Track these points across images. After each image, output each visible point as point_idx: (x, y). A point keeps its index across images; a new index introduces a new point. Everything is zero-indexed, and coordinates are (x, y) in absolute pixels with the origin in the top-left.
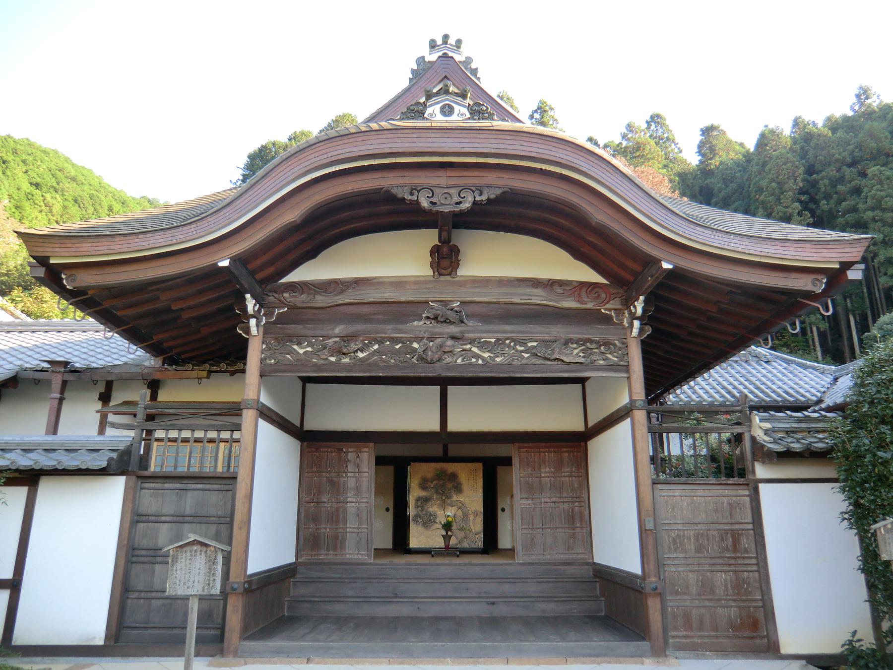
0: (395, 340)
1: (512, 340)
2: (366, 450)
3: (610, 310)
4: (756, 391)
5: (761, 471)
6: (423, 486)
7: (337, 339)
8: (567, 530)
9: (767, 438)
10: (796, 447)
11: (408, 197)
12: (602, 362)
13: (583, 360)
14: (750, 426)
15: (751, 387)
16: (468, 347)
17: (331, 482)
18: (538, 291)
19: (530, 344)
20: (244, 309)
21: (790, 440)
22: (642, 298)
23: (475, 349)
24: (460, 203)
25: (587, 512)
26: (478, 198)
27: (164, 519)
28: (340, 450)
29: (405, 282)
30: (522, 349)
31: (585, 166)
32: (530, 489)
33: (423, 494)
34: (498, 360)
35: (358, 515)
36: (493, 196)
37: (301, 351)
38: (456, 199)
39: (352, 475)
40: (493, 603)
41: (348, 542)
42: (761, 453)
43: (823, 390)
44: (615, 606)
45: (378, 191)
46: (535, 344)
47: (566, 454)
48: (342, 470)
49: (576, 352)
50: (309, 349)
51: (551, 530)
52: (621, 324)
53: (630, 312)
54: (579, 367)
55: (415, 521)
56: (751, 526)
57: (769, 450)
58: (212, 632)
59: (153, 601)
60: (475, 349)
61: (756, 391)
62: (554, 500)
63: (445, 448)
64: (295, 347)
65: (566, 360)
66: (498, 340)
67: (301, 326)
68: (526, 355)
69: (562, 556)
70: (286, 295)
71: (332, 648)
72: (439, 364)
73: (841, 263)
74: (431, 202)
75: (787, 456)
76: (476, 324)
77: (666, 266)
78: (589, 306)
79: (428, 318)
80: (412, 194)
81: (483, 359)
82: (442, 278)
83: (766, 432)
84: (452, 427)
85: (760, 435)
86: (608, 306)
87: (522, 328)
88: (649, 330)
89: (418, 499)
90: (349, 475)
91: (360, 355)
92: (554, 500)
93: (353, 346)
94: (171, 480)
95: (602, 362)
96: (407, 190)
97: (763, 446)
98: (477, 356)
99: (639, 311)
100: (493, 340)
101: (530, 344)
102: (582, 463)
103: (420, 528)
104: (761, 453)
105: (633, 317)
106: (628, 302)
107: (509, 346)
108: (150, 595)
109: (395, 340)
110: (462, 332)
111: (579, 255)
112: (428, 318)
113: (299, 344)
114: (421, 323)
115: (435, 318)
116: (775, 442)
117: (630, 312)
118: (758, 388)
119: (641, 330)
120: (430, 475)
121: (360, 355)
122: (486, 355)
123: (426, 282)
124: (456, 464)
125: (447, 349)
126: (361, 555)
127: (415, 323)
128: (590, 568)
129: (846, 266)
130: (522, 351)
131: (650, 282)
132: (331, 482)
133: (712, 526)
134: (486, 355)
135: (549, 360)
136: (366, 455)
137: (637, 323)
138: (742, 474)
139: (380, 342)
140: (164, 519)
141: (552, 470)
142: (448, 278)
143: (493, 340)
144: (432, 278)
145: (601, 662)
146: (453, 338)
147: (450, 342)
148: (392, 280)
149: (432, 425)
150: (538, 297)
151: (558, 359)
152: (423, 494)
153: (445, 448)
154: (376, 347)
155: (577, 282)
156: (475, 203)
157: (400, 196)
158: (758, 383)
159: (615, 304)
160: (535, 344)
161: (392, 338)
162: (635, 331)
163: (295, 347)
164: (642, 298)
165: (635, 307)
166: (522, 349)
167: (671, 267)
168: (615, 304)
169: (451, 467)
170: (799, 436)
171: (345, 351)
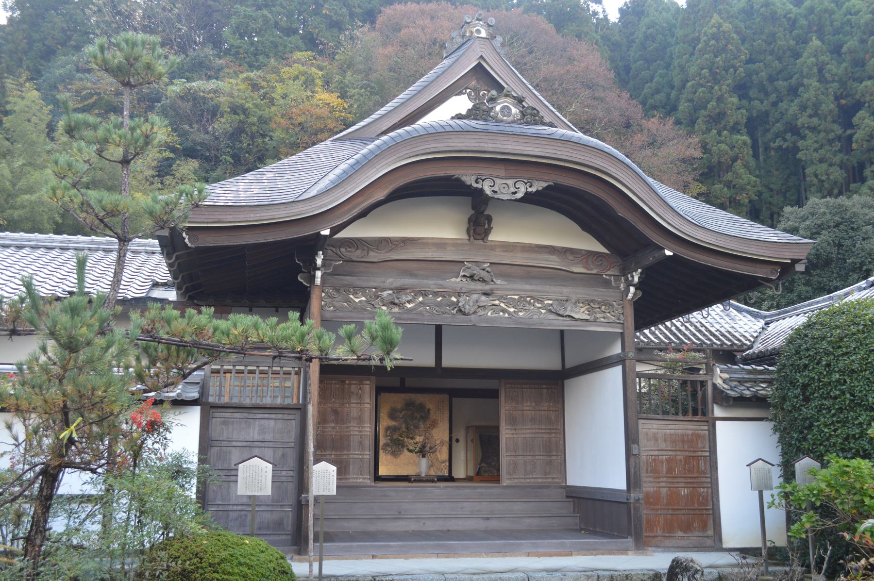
0: (436, 294)
1: (532, 297)
2: (368, 382)
3: (610, 275)
4: (698, 334)
5: (718, 412)
6: (392, 416)
7: (391, 292)
8: (545, 458)
9: (726, 386)
10: (747, 393)
11: (475, 185)
12: (602, 320)
13: (588, 317)
14: (712, 376)
15: (692, 329)
16: (497, 302)
17: (335, 412)
18: (554, 258)
19: (546, 302)
20: (314, 261)
21: (743, 388)
22: (640, 270)
23: (502, 305)
24: (515, 193)
25: (561, 442)
26: (530, 190)
27: (234, 444)
28: (343, 382)
29: (445, 244)
30: (539, 305)
31: (612, 170)
32: (513, 421)
33: (392, 423)
34: (521, 314)
35: (360, 443)
36: (540, 188)
37: (357, 300)
38: (513, 190)
39: (354, 405)
40: (488, 519)
41: (351, 467)
42: (722, 398)
43: (755, 335)
44: (597, 517)
45: (448, 178)
46: (550, 302)
47: (545, 391)
48: (345, 401)
49: (583, 309)
50: (363, 299)
51: (531, 458)
52: (618, 287)
53: (627, 279)
54: (584, 323)
55: (384, 449)
56: (708, 454)
57: (727, 395)
58: (284, 537)
59: (231, 513)
60: (502, 305)
61: (698, 334)
62: (534, 431)
63: (403, 381)
64: (351, 296)
65: (576, 316)
66: (521, 297)
67: (354, 278)
68: (543, 311)
69: (540, 480)
70: (343, 250)
71: (391, 547)
72: (473, 317)
73: (792, 260)
74: (493, 191)
75: (740, 401)
76: (503, 283)
77: (668, 253)
78: (594, 272)
79: (464, 276)
80: (477, 183)
81: (509, 313)
82: (476, 242)
83: (724, 381)
84: (446, 362)
85: (719, 382)
86: (608, 273)
87: (539, 288)
88: (640, 294)
89: (388, 428)
90: (352, 405)
91: (409, 306)
92: (534, 431)
93: (404, 298)
94: (241, 410)
95: (602, 320)
96: (474, 178)
97: (722, 392)
98: (504, 311)
99: (636, 279)
100: (516, 297)
101: (546, 302)
102: (559, 398)
103: (389, 457)
104: (722, 398)
105: (629, 284)
106: (625, 271)
107: (530, 303)
108: (227, 508)
109: (436, 294)
110: (492, 290)
111: (587, 227)
112: (464, 276)
113: (355, 294)
114: (459, 279)
115: (472, 277)
116: (732, 390)
117: (627, 279)
118: (700, 331)
119: (635, 294)
120: (399, 406)
121: (409, 306)
122: (512, 310)
123: (462, 245)
124: (424, 395)
125: (482, 304)
126: (364, 478)
127: (453, 280)
128: (563, 490)
129: (795, 261)
130: (539, 308)
131: (651, 259)
132: (335, 412)
133: (679, 453)
134: (512, 310)
135: (562, 316)
136: (368, 387)
137: (632, 289)
138: (704, 414)
139: (425, 294)
140: (234, 444)
141: (533, 404)
142: (481, 242)
143: (516, 297)
144: (467, 242)
145: (598, 554)
146: (486, 294)
147: (483, 298)
148: (435, 241)
149: (429, 361)
150: (553, 261)
151: (569, 316)
152: (392, 423)
153: (403, 381)
154: (421, 299)
155: (585, 251)
156: (527, 193)
157: (469, 183)
158: (698, 325)
159: (614, 271)
160: (550, 302)
161: (435, 292)
162: (630, 296)
163: (351, 296)
164: (640, 270)
165: (633, 277)
166: (539, 305)
167: (671, 254)
168: (614, 271)
169: (419, 398)
170: (748, 385)
171: (396, 301)
